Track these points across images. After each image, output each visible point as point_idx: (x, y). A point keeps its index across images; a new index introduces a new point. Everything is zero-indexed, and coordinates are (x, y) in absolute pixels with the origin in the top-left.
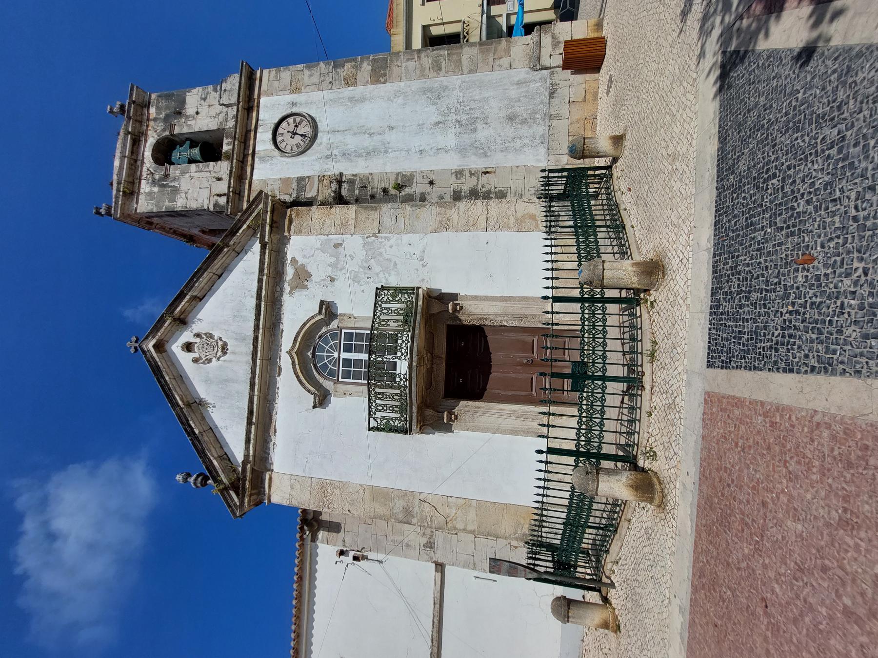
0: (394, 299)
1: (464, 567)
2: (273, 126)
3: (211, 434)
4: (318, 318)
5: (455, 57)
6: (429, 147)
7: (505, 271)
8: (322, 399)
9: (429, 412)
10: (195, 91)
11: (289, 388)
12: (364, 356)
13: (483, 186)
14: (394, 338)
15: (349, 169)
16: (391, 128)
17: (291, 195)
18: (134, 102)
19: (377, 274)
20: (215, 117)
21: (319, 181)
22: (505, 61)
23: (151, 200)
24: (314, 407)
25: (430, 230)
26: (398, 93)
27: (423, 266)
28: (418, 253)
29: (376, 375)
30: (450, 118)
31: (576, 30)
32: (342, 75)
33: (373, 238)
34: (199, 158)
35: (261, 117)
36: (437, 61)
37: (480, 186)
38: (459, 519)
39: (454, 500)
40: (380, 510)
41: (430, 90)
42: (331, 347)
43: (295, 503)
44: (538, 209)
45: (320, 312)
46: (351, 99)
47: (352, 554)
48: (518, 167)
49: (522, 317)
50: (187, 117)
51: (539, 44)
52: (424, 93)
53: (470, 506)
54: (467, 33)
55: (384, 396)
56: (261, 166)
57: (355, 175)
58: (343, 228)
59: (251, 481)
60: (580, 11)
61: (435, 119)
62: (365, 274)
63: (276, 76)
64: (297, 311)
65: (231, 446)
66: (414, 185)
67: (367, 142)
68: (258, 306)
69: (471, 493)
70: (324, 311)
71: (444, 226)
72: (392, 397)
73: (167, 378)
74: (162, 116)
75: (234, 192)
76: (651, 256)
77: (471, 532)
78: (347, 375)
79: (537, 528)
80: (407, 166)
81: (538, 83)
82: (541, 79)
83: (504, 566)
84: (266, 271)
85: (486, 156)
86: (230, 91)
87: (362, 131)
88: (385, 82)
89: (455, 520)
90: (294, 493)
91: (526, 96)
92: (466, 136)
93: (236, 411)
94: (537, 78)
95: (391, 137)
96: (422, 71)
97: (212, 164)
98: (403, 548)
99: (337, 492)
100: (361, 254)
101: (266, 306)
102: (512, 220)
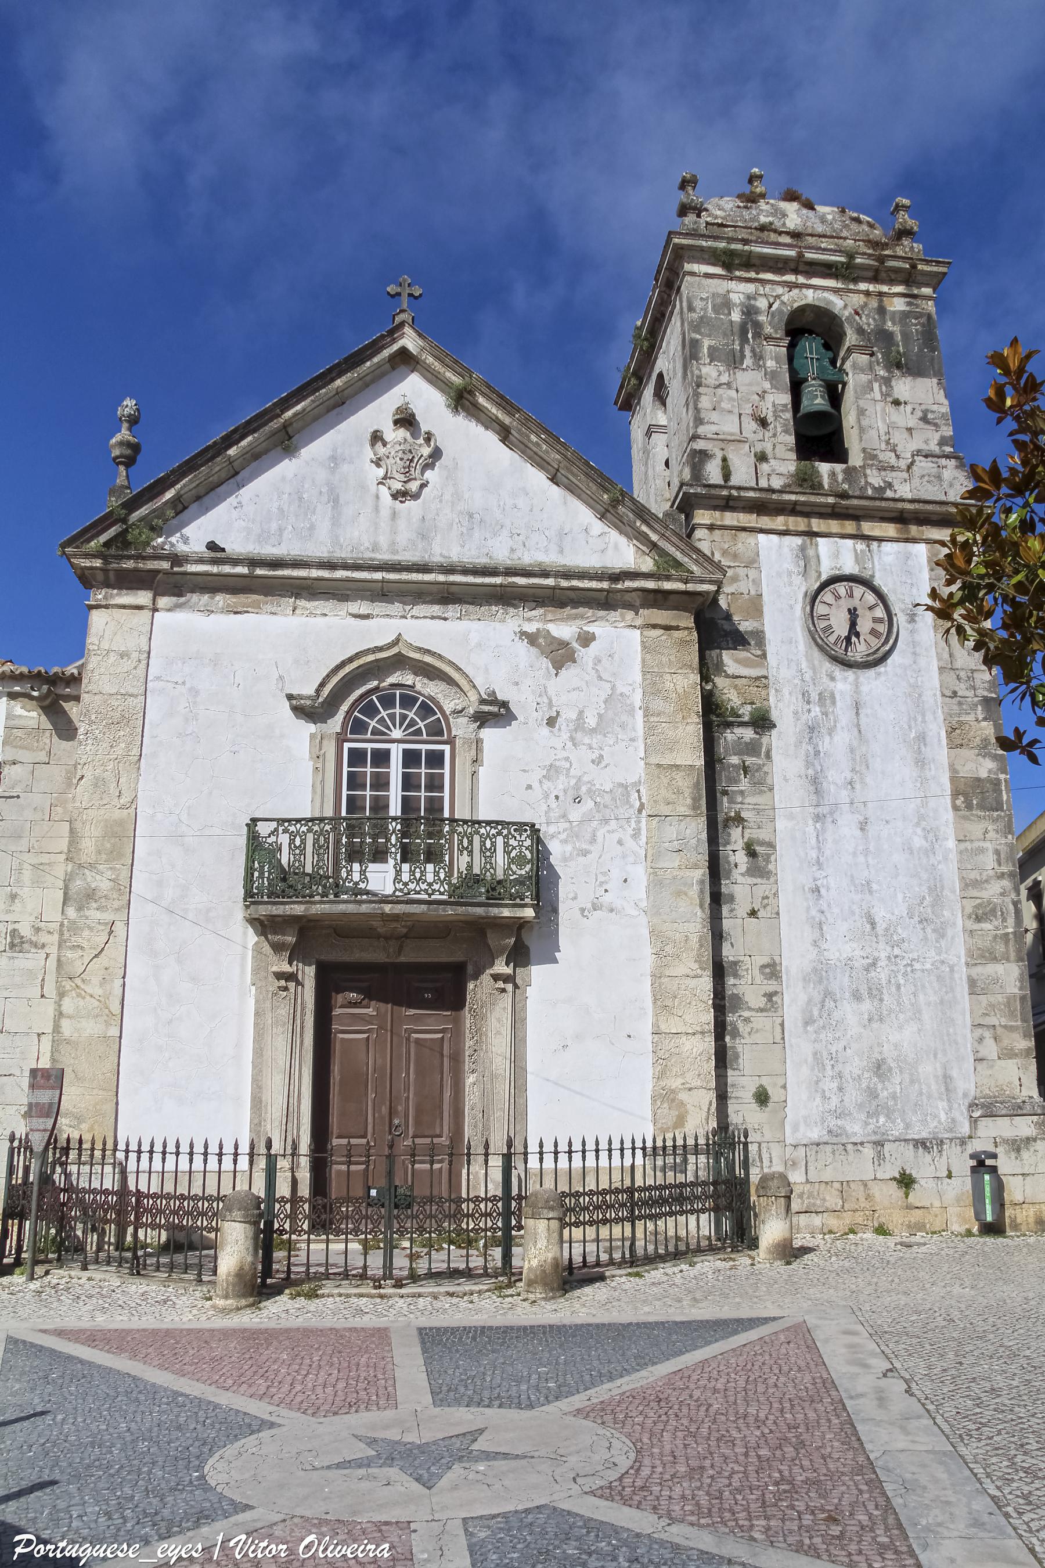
3: (223, 475)
5: (1000, 948)
6: (825, 907)
7: (578, 1064)
10: (941, 397)
13: (747, 1020)
14: (433, 856)
15: (781, 740)
18: (914, 267)
20: (888, 442)
21: (757, 678)
22: (990, 1049)
23: (714, 306)
24: (290, 697)
26: (933, 835)
27: (582, 910)
28: (607, 899)
29: (358, 830)
30: (882, 945)
32: (971, 718)
33: (637, 804)
35: (887, 547)
38: (81, 1003)
40: (88, 846)
41: (938, 901)
42: (413, 723)
43: (93, 662)
46: (922, 738)
48: (784, 1087)
50: (887, 382)
53: (107, 1024)
56: (786, 550)
57: (768, 756)
59: (136, 570)
61: (881, 914)
62: (565, 791)
65: (202, 520)
66: (751, 880)
67: (835, 777)
68: (492, 572)
73: (338, 383)
74: (889, 325)
75: (729, 498)
77: (57, 1028)
78: (357, 757)
80: (787, 864)
81: (945, 1115)
82: (953, 1120)
83: (45, 1097)
84: (564, 583)
85: (806, 1023)
86: (939, 477)
87: (860, 763)
88: (956, 808)
89: (79, 995)
90: (113, 658)
91: (921, 1094)
92: (846, 979)
93: (274, 526)
94: (956, 1114)
95: (847, 825)
96: (976, 884)
97: (791, 439)
101: (495, 586)
102: (676, 1083)
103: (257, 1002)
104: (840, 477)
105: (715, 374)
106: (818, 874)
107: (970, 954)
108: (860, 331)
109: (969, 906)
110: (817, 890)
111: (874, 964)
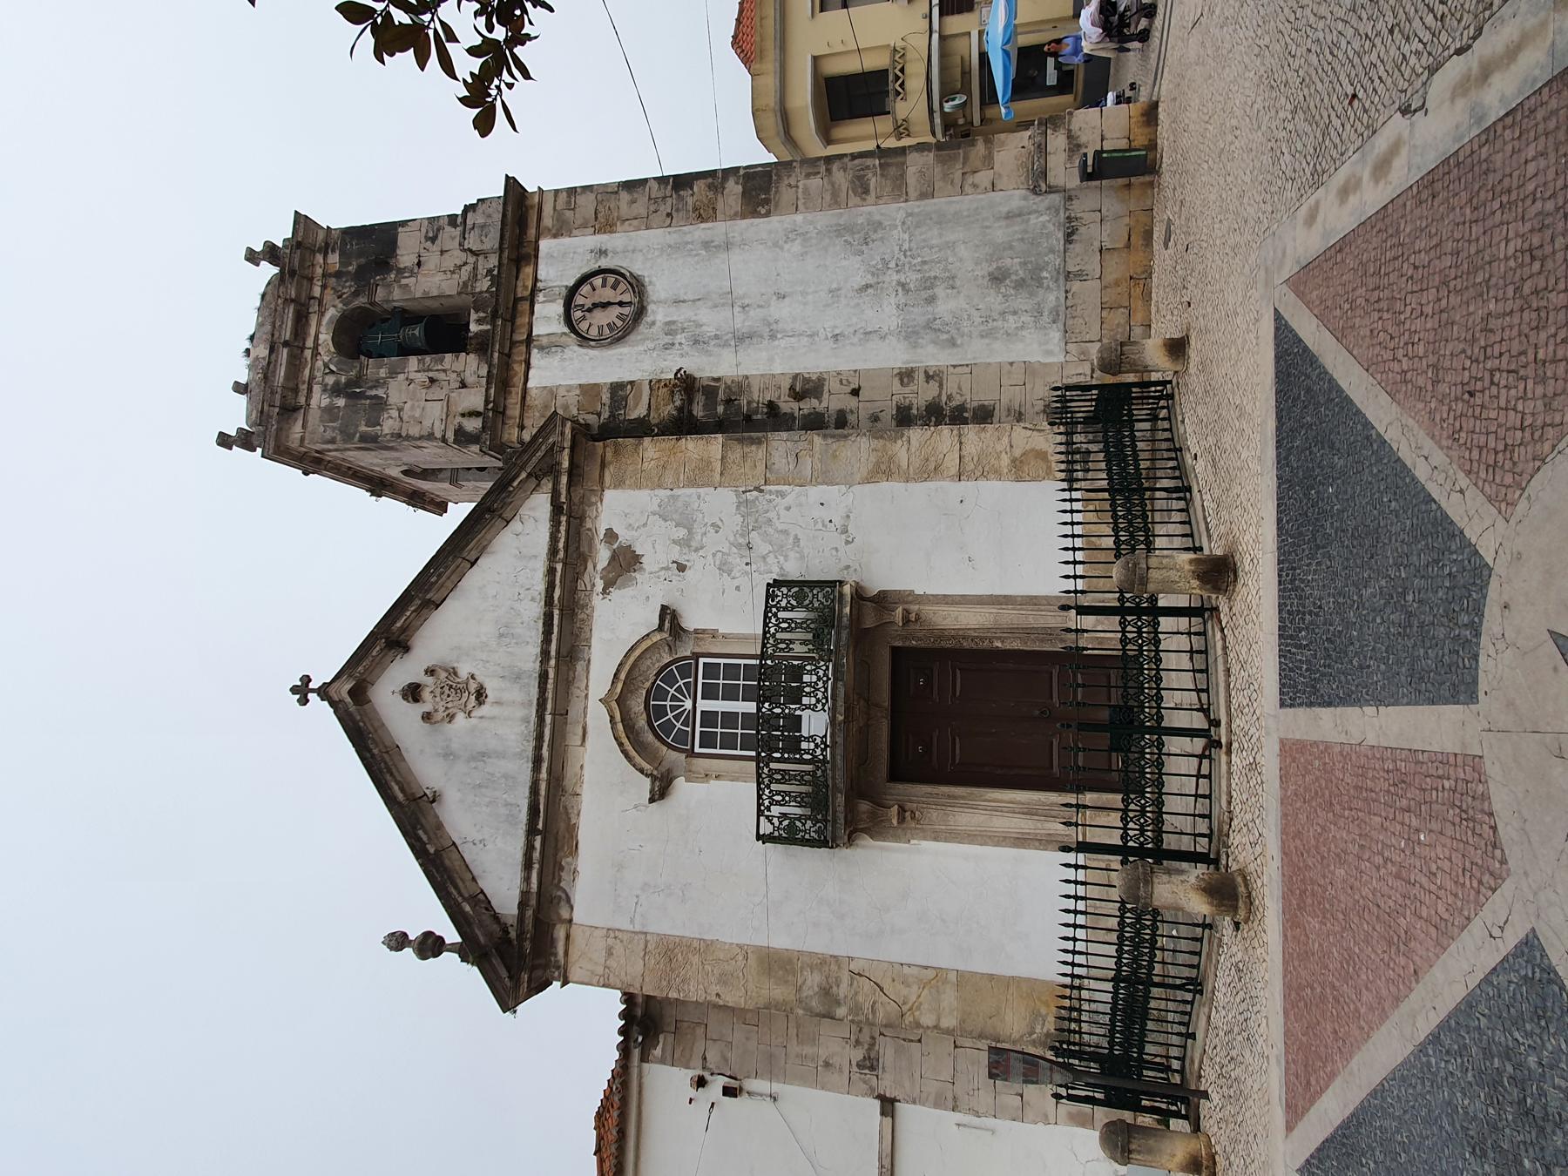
0: (800, 604)
1: (937, 1105)
2: (564, 292)
4: (657, 637)
5: (892, 171)
6: (851, 330)
7: (993, 547)
8: (661, 789)
9: (864, 806)
11: (602, 773)
12: (751, 707)
13: (950, 397)
17: (599, 414)
19: (764, 558)
20: (453, 272)
22: (983, 177)
25: (858, 477)
26: (791, 234)
28: (838, 521)
29: (770, 740)
30: (887, 279)
32: (690, 201)
35: (542, 274)
36: (860, 178)
37: (944, 398)
38: (925, 1006)
39: (915, 971)
40: (780, 993)
41: (850, 229)
44: (1048, 441)
45: (660, 628)
46: (706, 245)
47: (722, 1081)
48: (1011, 364)
49: (1028, 632)
50: (400, 271)
52: (839, 234)
53: (945, 981)
54: (902, 70)
55: (786, 777)
56: (542, 363)
57: (718, 380)
58: (699, 477)
61: (859, 280)
63: (569, 202)
64: (617, 624)
66: (826, 395)
69: (946, 958)
70: (667, 625)
71: (883, 471)
72: (799, 778)
76: (1219, 552)
77: (949, 1032)
78: (707, 740)
79: (1067, 992)
80: (812, 362)
83: (1017, 1066)
86: (483, 227)
88: (768, 214)
89: (918, 1008)
90: (612, 963)
94: (1042, 207)
97: (449, 357)
98: (820, 1073)
99: (695, 959)
100: (733, 522)
102: (1005, 460)
103: (925, 839)
107: (896, 199)
109: (854, 200)
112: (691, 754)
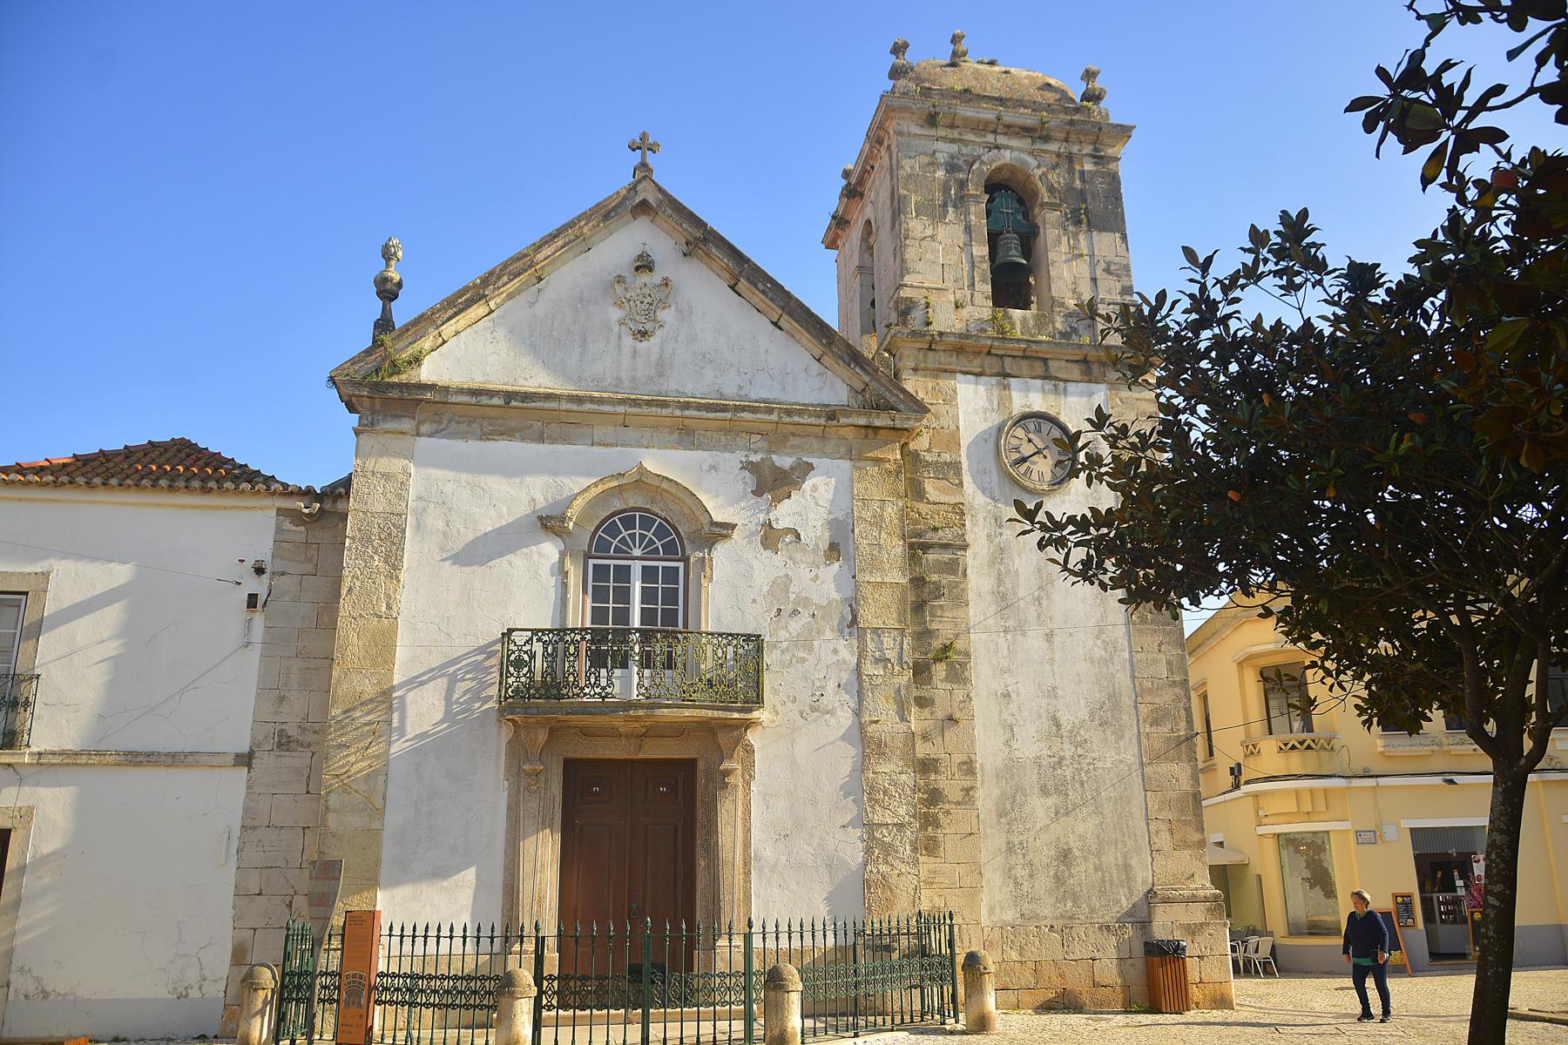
1: (246, 809)
2: (1052, 412)
6: (1015, 710)
11: (570, 477)
12: (636, 622)
16: (1049, 637)
20: (1074, 291)
22: (1164, 841)
29: (606, 647)
30: (1066, 746)
31: (1210, 956)
34: (998, 261)
38: (347, 797)
41: (1116, 707)
51: (1193, 899)
54: (1309, 747)
57: (965, 575)
60: (1406, 980)
61: (1065, 719)
64: (713, 483)
78: (601, 572)
92: (1035, 777)
95: (1034, 640)
104: (1031, 323)
105: (920, 227)
106: (1009, 682)
108: (1051, 189)
110: (1007, 695)
111: (1059, 763)
112: (588, 556)
